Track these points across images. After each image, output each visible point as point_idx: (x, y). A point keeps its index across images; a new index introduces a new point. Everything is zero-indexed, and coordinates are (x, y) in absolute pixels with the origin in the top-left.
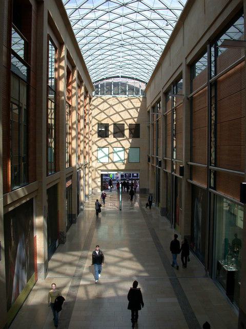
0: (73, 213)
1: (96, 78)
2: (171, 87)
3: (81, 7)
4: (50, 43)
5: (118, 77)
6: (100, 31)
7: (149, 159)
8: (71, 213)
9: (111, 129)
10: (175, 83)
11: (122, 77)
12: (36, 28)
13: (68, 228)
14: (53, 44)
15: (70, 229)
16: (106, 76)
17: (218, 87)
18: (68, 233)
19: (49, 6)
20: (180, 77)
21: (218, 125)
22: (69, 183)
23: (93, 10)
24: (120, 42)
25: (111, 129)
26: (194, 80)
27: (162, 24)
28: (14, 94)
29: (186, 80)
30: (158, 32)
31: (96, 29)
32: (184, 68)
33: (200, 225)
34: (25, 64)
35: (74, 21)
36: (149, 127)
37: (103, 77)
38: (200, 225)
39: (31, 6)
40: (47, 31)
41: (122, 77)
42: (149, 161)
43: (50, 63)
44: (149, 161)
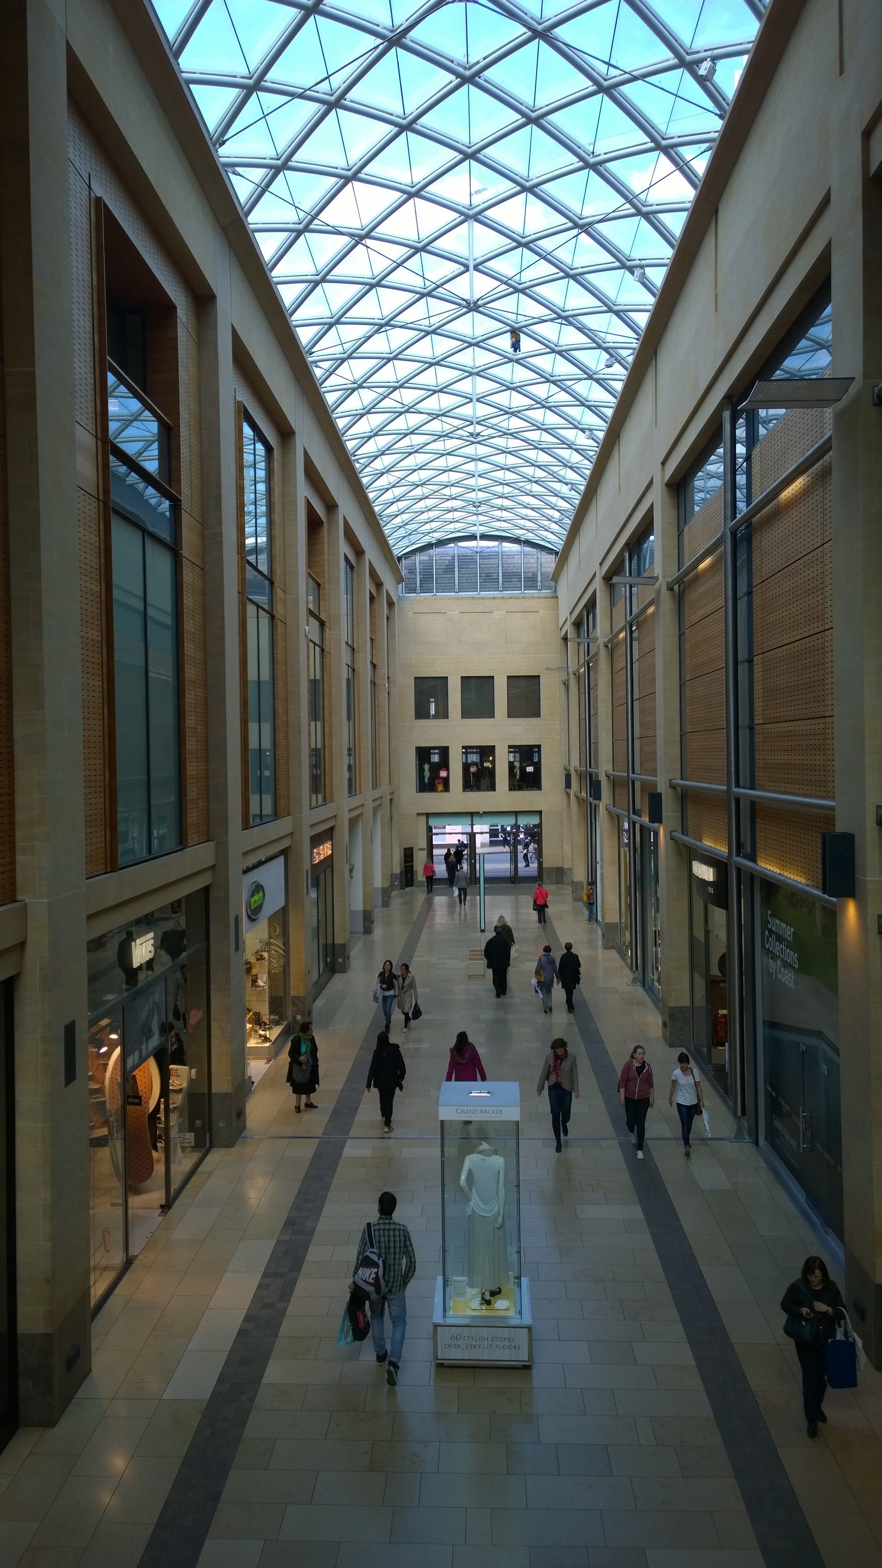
0: (338, 940)
1: (405, 542)
2: (623, 561)
3: (343, 320)
4: (247, 431)
5: (473, 537)
6: (408, 396)
7: (568, 777)
8: (330, 941)
9: (502, 762)
10: (637, 542)
11: (484, 537)
12: (283, 495)
13: (319, 988)
14: (259, 436)
15: (326, 991)
16: (437, 535)
17: (755, 543)
18: (320, 1003)
19: (63, 15)
20: (646, 528)
21: (757, 660)
22: (325, 850)
23: (381, 326)
24: (470, 429)
25: (502, 762)
26: (686, 529)
27: (595, 360)
28: (125, 577)
29: (663, 536)
30: (585, 388)
31: (395, 388)
32: (657, 497)
33: (426, 780)
34: (164, 492)
35: (326, 365)
36: (566, 684)
37: (427, 539)
38: (426, 780)
39: (171, 308)
40: (231, 389)
41: (484, 537)
42: (568, 785)
43: (262, 509)
44: (568, 785)
